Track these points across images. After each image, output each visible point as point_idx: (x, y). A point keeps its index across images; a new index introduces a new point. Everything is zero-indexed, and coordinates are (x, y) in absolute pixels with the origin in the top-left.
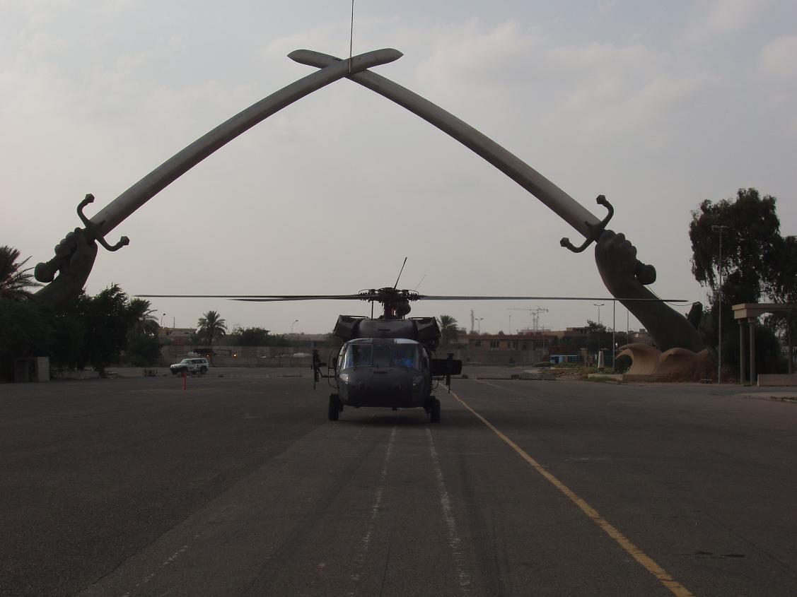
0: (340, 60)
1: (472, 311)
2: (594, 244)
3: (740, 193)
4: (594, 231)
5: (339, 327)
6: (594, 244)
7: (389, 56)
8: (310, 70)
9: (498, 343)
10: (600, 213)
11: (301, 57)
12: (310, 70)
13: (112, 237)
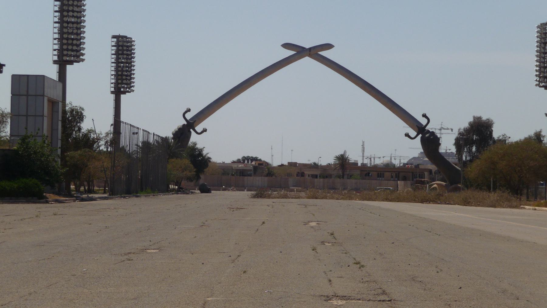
0: (305, 48)
1: (363, 142)
2: (420, 135)
3: (474, 117)
4: (421, 129)
5: (237, 160)
6: (420, 135)
7: (328, 46)
8: (291, 53)
9: (383, 174)
10: (424, 121)
11: (287, 46)
12: (291, 53)
13: (199, 128)
